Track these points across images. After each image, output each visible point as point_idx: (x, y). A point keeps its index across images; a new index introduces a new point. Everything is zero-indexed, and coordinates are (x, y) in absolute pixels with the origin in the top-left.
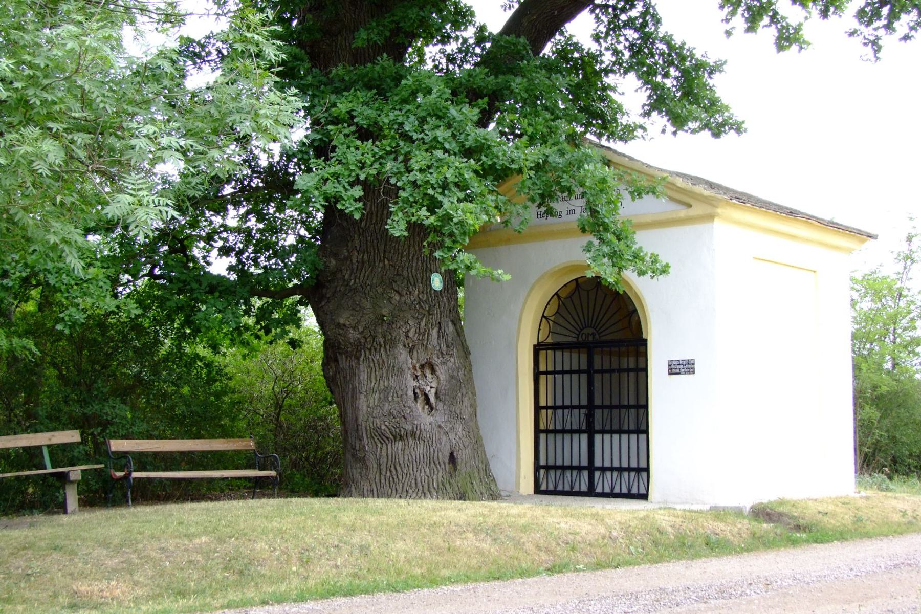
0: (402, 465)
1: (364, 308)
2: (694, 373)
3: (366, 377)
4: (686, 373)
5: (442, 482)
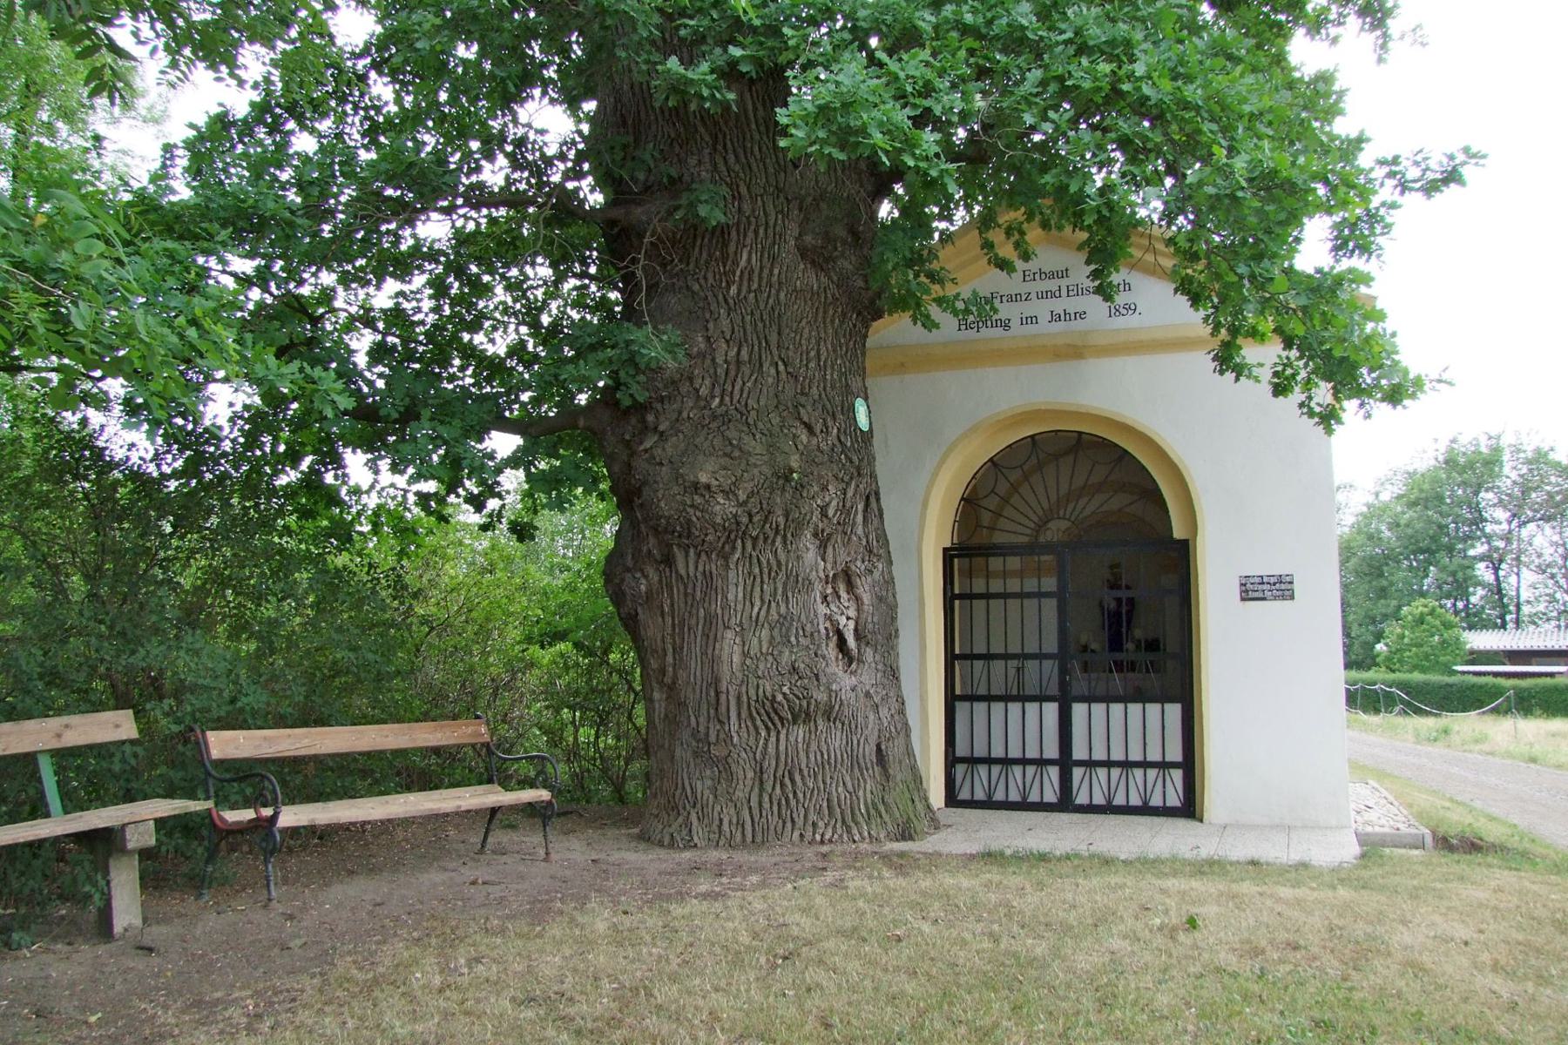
0: (806, 773)
1: (749, 453)
2: (1292, 597)
3: (741, 595)
4: (1275, 598)
5: (874, 803)
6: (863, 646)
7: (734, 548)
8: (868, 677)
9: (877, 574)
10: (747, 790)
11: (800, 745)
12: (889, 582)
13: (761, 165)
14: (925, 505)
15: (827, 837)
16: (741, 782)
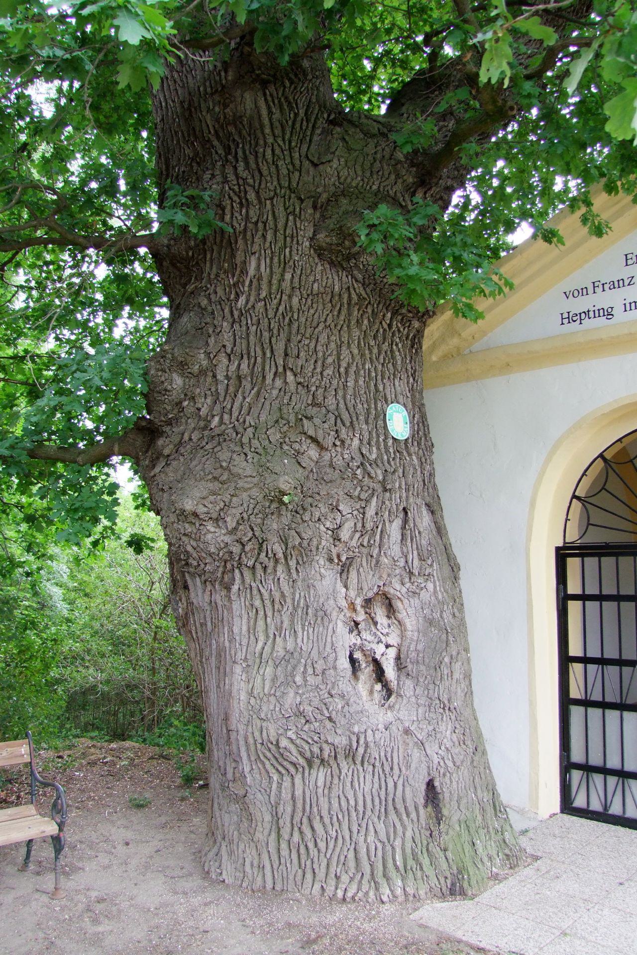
3: (245, 628)
6: (403, 678)
10: (266, 832)
11: (320, 791)
13: (273, 169)
15: (349, 894)
16: (259, 824)
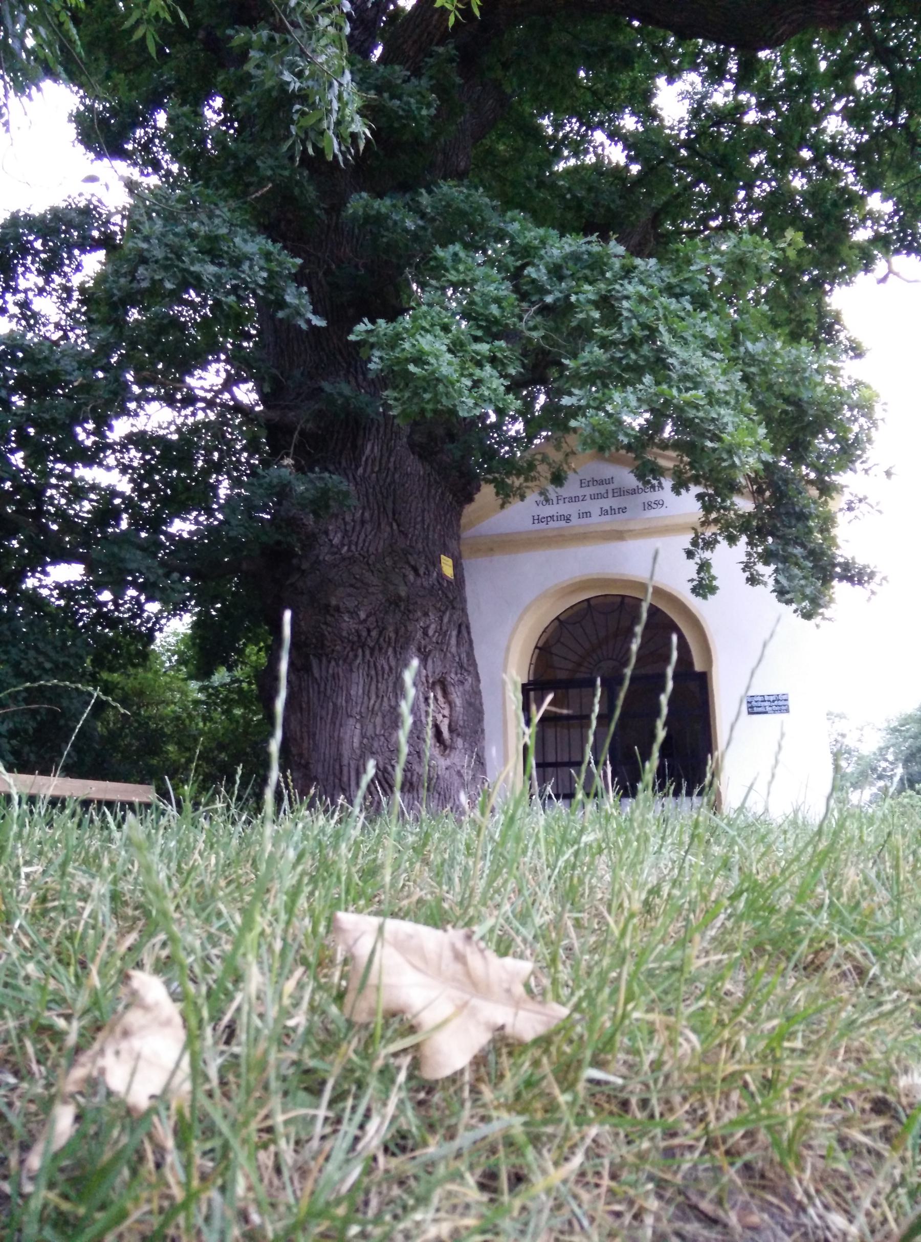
2: (787, 711)
4: (775, 712)
7: (356, 656)
8: (460, 759)
9: (467, 686)
12: (477, 693)
14: (508, 649)
